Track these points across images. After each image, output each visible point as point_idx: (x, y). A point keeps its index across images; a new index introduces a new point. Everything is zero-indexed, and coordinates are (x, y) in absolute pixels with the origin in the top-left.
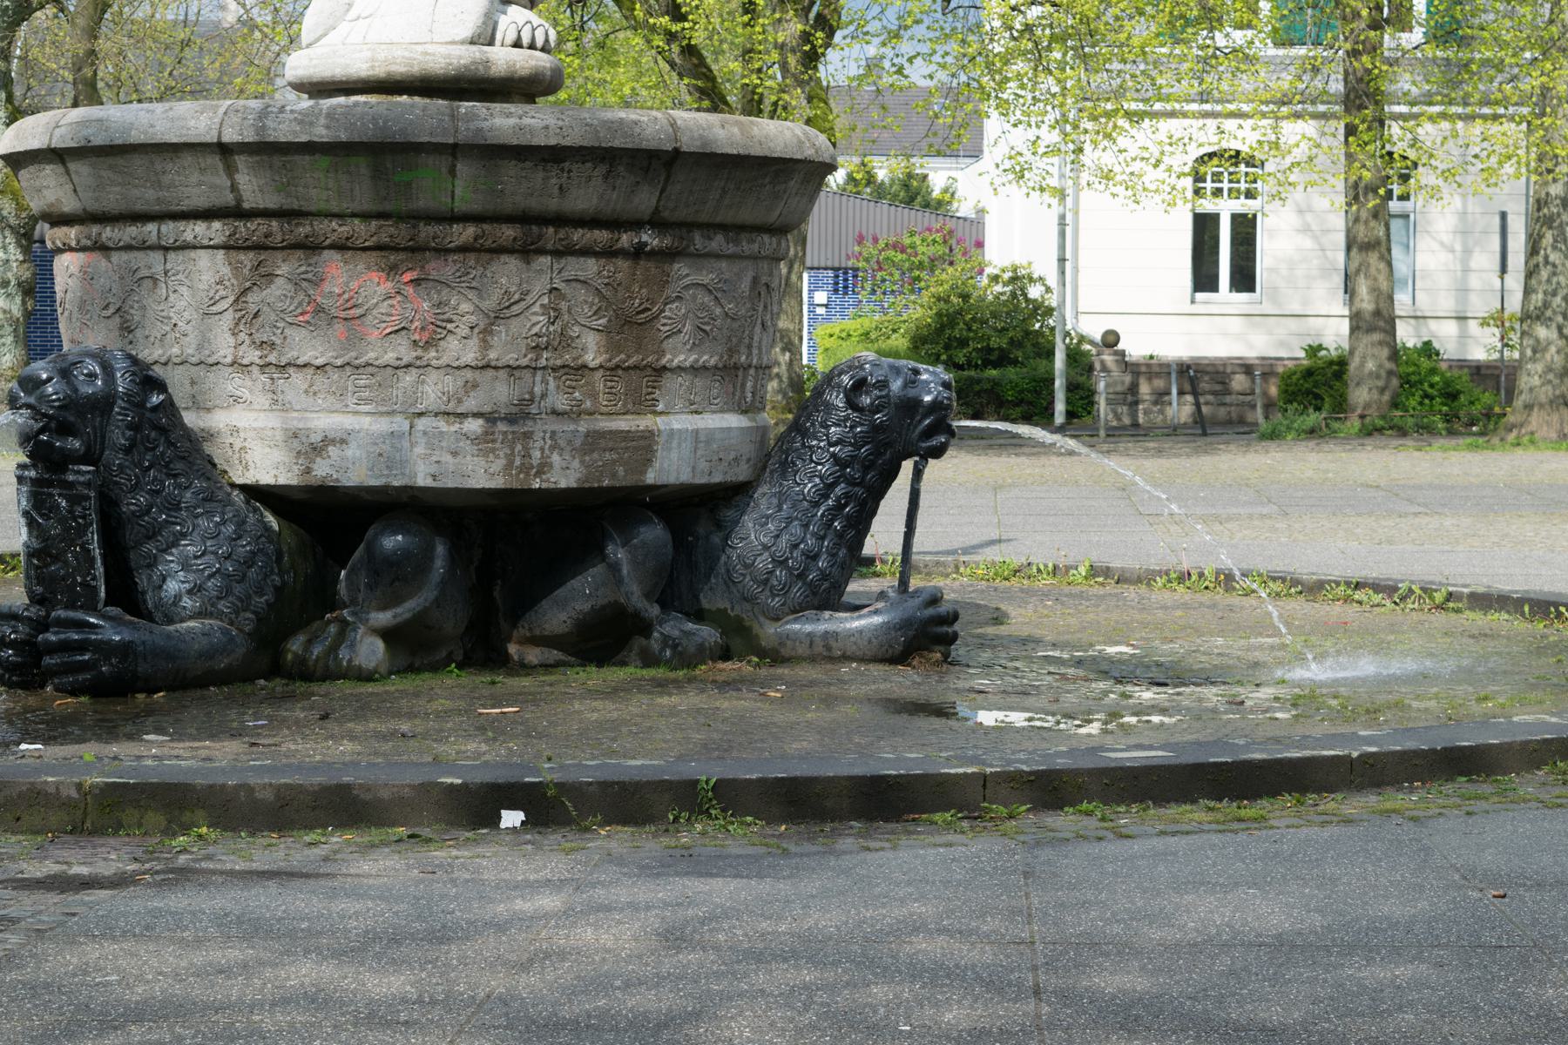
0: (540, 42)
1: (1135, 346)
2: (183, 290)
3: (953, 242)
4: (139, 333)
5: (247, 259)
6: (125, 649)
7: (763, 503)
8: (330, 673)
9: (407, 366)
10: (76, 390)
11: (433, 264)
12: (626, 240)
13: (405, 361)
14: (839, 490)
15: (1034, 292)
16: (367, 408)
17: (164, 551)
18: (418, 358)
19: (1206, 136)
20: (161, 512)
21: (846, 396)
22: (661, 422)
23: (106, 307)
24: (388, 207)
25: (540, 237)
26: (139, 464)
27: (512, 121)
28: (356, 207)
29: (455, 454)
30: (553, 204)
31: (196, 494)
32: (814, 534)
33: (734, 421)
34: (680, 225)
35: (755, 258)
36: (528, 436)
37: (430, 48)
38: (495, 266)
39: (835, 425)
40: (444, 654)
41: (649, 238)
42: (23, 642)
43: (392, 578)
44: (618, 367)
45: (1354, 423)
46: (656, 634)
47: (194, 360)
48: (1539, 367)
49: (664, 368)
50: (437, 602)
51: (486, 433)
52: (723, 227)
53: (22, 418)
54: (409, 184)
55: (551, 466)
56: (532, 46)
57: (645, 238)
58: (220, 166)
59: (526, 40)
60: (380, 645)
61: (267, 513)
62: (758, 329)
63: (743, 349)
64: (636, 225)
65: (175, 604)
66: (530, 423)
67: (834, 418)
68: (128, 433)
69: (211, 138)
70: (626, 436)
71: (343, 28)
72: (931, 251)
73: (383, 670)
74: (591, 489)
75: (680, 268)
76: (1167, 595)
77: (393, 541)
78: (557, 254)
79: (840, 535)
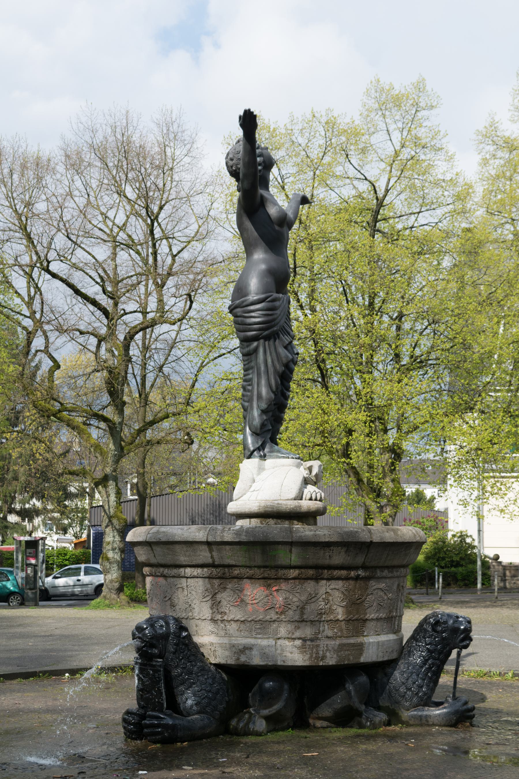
0: (318, 498)
1: (505, 559)
2: (193, 592)
3: (437, 521)
4: (177, 607)
5: (216, 582)
6: (173, 727)
7: (402, 666)
8: (247, 733)
9: (274, 621)
10: (156, 632)
11: (283, 584)
12: (353, 574)
13: (274, 619)
15: (468, 540)
16: (260, 636)
17: (187, 689)
18: (278, 618)
20: (186, 675)
21: (432, 627)
22: (366, 640)
23: (165, 597)
24: (267, 564)
25: (322, 574)
26: (178, 658)
27: (312, 533)
29: (291, 653)
30: (327, 562)
31: (198, 668)
32: (421, 678)
33: (392, 637)
34: (372, 567)
35: (398, 577)
37: (280, 502)
38: (306, 584)
39: (428, 637)
40: (286, 724)
41: (361, 572)
42: (137, 723)
43: (267, 698)
44: (350, 620)
46: (364, 716)
47: (197, 618)
49: (367, 619)
50: (285, 707)
51: (303, 645)
52: (387, 567)
53: (137, 642)
54: (275, 556)
55: (326, 657)
56: (316, 500)
57: (360, 573)
58: (207, 549)
59: (314, 498)
60: (264, 722)
61: (223, 674)
62: (399, 603)
63: (394, 610)
64: (356, 568)
65: (191, 709)
66: (318, 641)
67: (428, 635)
68: (175, 647)
69: (204, 539)
70: (353, 645)
71: (248, 494)
72: (430, 524)
73: (265, 732)
74: (341, 665)
75: (372, 583)
77: (269, 684)
78: (328, 579)
79: (430, 678)
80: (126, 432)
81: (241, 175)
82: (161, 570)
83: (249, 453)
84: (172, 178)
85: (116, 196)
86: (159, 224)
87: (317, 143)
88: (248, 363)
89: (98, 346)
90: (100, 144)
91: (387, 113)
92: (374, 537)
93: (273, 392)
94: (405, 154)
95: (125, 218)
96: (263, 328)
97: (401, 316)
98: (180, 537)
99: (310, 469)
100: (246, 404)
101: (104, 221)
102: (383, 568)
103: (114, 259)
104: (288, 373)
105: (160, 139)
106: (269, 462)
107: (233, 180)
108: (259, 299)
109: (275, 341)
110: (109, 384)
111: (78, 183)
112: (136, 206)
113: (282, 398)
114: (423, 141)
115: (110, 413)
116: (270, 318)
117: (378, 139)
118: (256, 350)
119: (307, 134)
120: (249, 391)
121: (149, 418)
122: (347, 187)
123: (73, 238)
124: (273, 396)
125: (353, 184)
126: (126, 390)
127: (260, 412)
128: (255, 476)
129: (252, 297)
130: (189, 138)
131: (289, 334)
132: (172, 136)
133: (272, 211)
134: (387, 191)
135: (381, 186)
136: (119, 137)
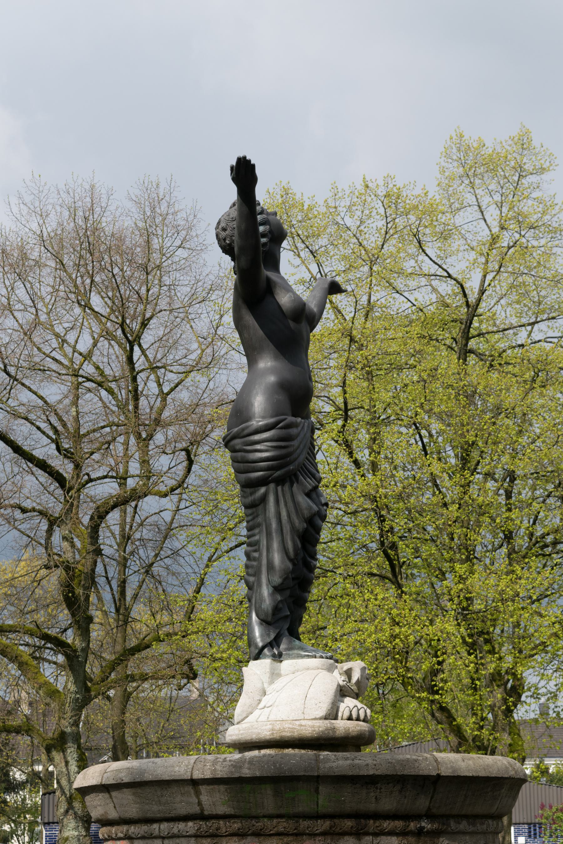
0: (362, 717)
12: (413, 826)
25: (366, 825)
27: (349, 762)
30: (372, 807)
34: (442, 816)
35: (484, 833)
37: (303, 723)
41: (426, 825)
52: (466, 817)
56: (358, 719)
57: (423, 824)
58: (192, 791)
59: (354, 716)
64: (418, 817)
71: (257, 713)
78: (376, 835)
80: (93, 668)
81: (236, 249)
82: (125, 828)
83: (257, 651)
84: (160, 280)
85: (77, 310)
86: (143, 352)
87: (374, 225)
88: (254, 519)
89: (50, 532)
90: (52, 234)
91: (477, 181)
92: (443, 769)
93: (291, 560)
94: (505, 240)
95: (92, 341)
96: (278, 469)
97: (512, 476)
98: (152, 775)
99: (348, 673)
100: (251, 579)
101: (61, 348)
102: (459, 817)
103: (75, 403)
104: (313, 532)
105: (141, 224)
106: (287, 665)
107: (228, 258)
108: (266, 425)
109: (292, 486)
110: (67, 587)
111: (21, 292)
112: (109, 324)
113: (305, 570)
114: (533, 219)
115: (70, 637)
116: (283, 451)
117: (466, 218)
118: (264, 499)
119: (359, 213)
120: (255, 559)
121: (133, 642)
122: (423, 290)
123: (12, 370)
124: (290, 566)
125: (431, 285)
126: (93, 598)
127: (271, 590)
128: (266, 685)
129: (257, 422)
130: (184, 222)
131: (314, 476)
132: (158, 220)
133: (284, 300)
134: (482, 292)
135: (473, 285)
136: (81, 222)
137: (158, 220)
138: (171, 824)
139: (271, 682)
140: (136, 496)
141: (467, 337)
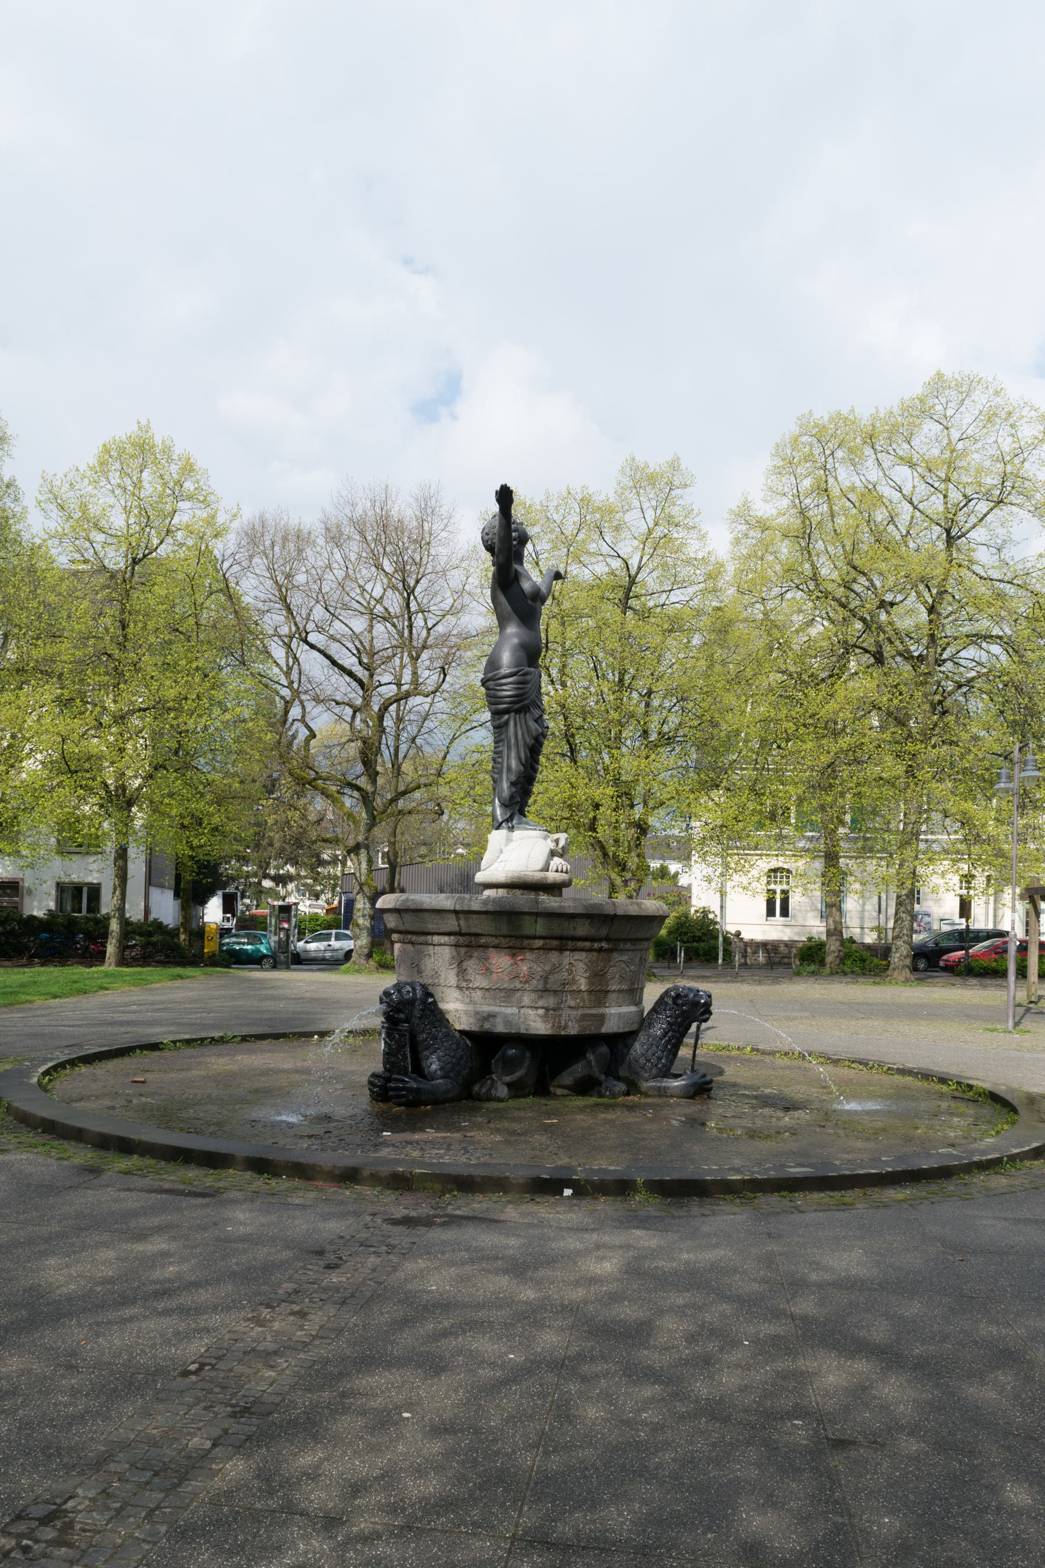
1: (746, 936)
5: (463, 950)
12: (596, 945)
14: (670, 1034)
15: (711, 916)
19: (774, 863)
28: (501, 933)
30: (571, 933)
36: (560, 1016)
41: (604, 945)
43: (510, 1065)
45: (827, 970)
48: (898, 955)
52: (630, 940)
60: (506, 1089)
64: (600, 940)
70: (595, 1015)
75: (615, 955)
76: (781, 1061)
77: (512, 1052)
78: (572, 950)
79: (670, 1050)
80: (379, 802)
81: (496, 550)
85: (373, 569)
86: (415, 598)
89: (354, 717)
91: (642, 491)
94: (658, 532)
96: (515, 704)
97: (650, 693)
99: (557, 841)
100: (496, 776)
101: (362, 594)
103: (370, 631)
106: (517, 834)
107: (488, 555)
111: (337, 556)
115: (363, 782)
118: (507, 723)
122: (600, 564)
123: (332, 610)
124: (522, 768)
126: (379, 760)
129: (505, 671)
132: (429, 511)
133: (526, 586)
135: (634, 563)
136: (378, 511)
137: (429, 511)
138: (440, 937)
139: (507, 845)
140: (407, 696)
141: (627, 598)
